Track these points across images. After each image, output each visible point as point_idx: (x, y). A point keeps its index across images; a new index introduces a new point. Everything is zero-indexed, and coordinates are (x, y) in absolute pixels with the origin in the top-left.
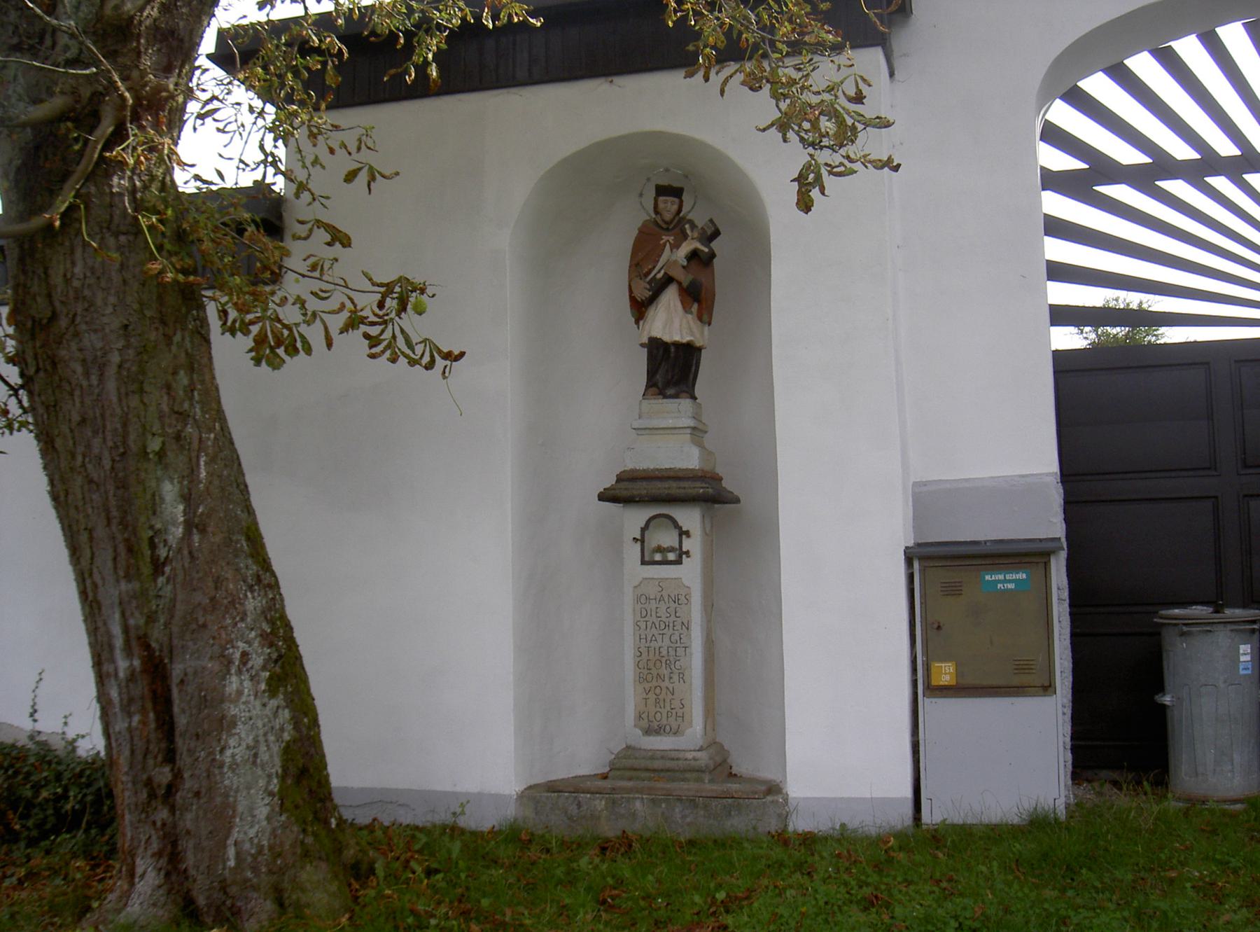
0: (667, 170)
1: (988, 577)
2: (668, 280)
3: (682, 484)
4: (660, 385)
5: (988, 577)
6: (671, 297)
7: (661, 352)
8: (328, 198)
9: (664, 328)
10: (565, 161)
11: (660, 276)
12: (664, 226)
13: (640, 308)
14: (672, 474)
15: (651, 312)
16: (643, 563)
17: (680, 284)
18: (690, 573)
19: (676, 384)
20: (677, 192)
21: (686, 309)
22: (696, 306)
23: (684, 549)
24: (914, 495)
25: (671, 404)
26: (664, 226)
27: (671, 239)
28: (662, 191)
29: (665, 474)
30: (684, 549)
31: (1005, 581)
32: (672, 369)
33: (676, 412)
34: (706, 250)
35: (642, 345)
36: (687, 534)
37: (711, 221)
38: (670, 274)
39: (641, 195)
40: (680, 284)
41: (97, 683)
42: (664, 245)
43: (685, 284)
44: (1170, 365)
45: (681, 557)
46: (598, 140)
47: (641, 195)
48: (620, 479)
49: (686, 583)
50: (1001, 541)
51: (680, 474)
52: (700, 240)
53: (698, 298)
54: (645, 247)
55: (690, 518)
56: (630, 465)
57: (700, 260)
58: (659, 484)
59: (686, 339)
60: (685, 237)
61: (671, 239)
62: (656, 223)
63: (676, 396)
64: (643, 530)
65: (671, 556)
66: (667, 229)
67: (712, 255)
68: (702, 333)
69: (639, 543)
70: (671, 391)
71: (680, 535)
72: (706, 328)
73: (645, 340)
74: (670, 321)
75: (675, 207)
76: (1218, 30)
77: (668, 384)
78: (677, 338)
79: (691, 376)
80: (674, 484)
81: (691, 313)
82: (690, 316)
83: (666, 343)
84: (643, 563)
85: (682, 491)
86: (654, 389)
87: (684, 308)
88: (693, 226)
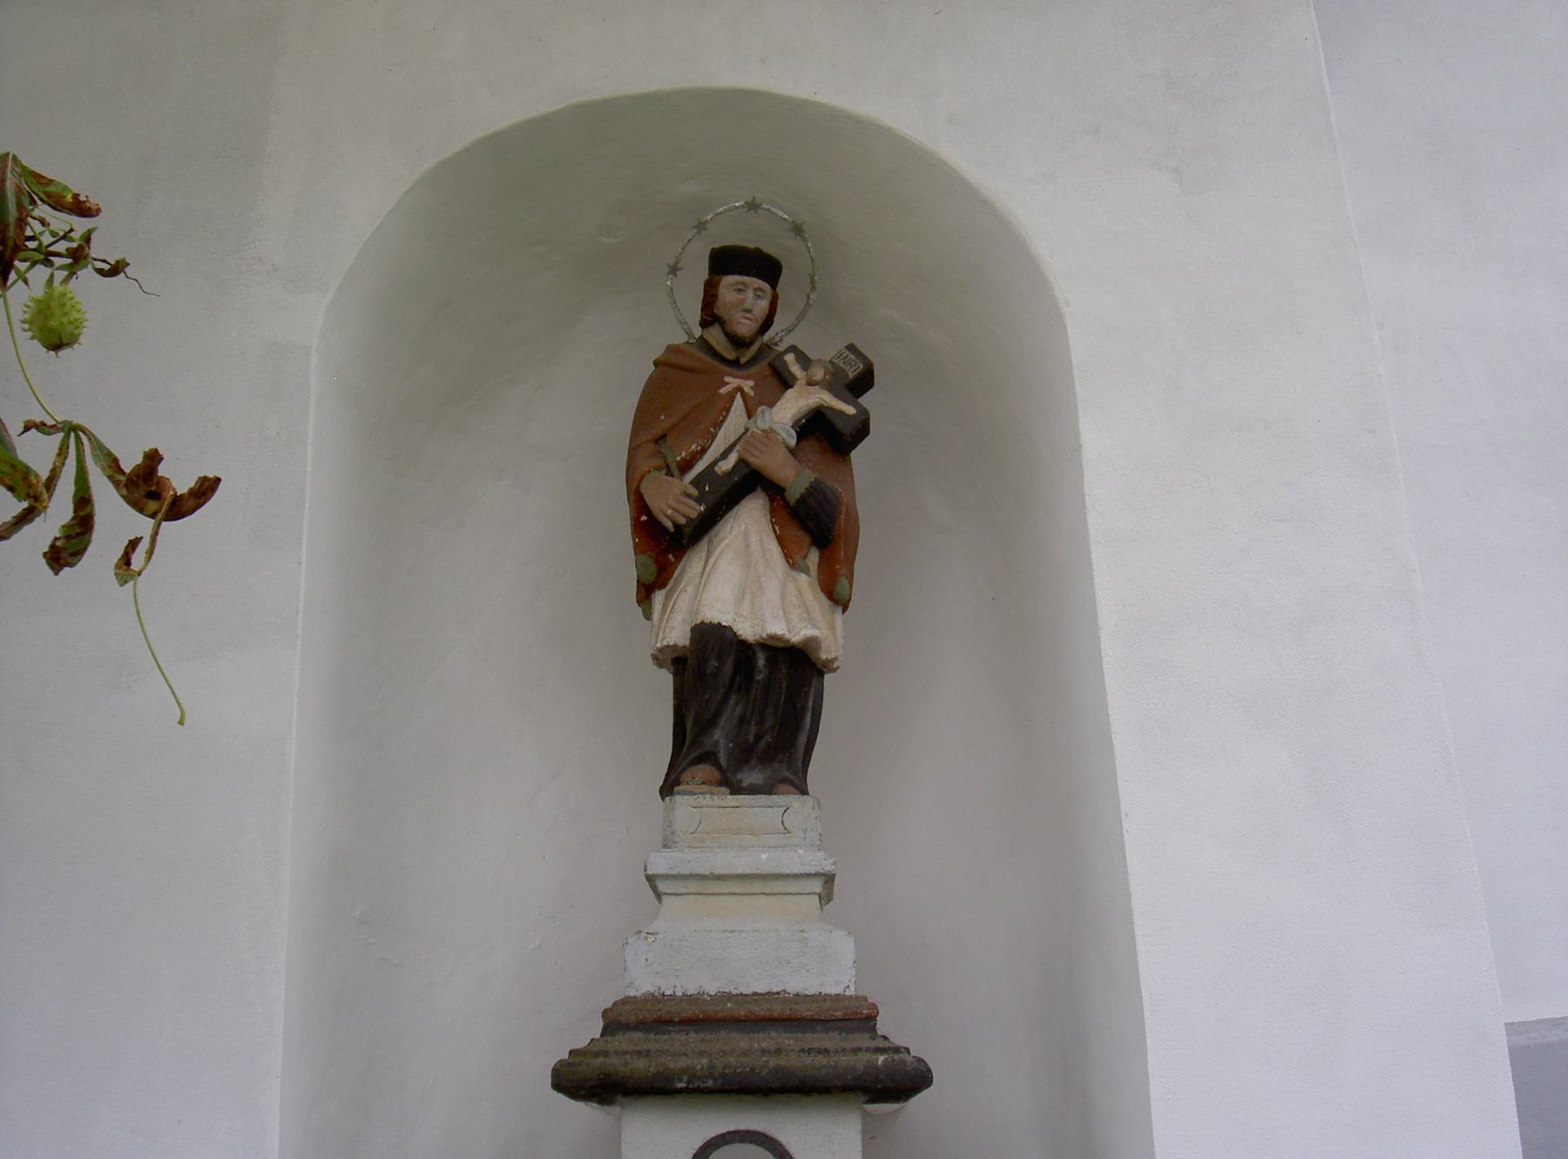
0: (753, 206)
2: (748, 481)
4: (722, 757)
6: (749, 527)
7: (728, 667)
9: (739, 600)
10: (496, 144)
11: (727, 465)
12: (729, 354)
13: (664, 547)
14: (777, 1010)
15: (693, 563)
17: (774, 491)
19: (767, 758)
20: (766, 267)
21: (792, 560)
22: (814, 556)
25: (759, 811)
26: (729, 354)
27: (748, 385)
28: (726, 261)
29: (760, 1010)
32: (744, 715)
33: (748, 831)
35: (660, 657)
37: (851, 348)
39: (674, 270)
41: (675, 734)
42: (731, 398)
43: (795, 492)
44: (670, 1022)
46: (592, 96)
47: (674, 270)
51: (804, 1011)
53: (818, 530)
54: (673, 403)
57: (828, 436)
58: (742, 1040)
59: (798, 633)
60: (785, 382)
61: (748, 385)
62: (704, 344)
63: (768, 789)
66: (735, 364)
67: (862, 429)
68: (832, 626)
70: (752, 777)
72: (839, 618)
73: (677, 634)
74: (745, 584)
75: (763, 305)
77: (745, 755)
78: (776, 627)
79: (802, 740)
80: (788, 1040)
81: (806, 571)
82: (803, 578)
83: (743, 644)
85: (821, 1060)
86: (704, 771)
87: (788, 556)
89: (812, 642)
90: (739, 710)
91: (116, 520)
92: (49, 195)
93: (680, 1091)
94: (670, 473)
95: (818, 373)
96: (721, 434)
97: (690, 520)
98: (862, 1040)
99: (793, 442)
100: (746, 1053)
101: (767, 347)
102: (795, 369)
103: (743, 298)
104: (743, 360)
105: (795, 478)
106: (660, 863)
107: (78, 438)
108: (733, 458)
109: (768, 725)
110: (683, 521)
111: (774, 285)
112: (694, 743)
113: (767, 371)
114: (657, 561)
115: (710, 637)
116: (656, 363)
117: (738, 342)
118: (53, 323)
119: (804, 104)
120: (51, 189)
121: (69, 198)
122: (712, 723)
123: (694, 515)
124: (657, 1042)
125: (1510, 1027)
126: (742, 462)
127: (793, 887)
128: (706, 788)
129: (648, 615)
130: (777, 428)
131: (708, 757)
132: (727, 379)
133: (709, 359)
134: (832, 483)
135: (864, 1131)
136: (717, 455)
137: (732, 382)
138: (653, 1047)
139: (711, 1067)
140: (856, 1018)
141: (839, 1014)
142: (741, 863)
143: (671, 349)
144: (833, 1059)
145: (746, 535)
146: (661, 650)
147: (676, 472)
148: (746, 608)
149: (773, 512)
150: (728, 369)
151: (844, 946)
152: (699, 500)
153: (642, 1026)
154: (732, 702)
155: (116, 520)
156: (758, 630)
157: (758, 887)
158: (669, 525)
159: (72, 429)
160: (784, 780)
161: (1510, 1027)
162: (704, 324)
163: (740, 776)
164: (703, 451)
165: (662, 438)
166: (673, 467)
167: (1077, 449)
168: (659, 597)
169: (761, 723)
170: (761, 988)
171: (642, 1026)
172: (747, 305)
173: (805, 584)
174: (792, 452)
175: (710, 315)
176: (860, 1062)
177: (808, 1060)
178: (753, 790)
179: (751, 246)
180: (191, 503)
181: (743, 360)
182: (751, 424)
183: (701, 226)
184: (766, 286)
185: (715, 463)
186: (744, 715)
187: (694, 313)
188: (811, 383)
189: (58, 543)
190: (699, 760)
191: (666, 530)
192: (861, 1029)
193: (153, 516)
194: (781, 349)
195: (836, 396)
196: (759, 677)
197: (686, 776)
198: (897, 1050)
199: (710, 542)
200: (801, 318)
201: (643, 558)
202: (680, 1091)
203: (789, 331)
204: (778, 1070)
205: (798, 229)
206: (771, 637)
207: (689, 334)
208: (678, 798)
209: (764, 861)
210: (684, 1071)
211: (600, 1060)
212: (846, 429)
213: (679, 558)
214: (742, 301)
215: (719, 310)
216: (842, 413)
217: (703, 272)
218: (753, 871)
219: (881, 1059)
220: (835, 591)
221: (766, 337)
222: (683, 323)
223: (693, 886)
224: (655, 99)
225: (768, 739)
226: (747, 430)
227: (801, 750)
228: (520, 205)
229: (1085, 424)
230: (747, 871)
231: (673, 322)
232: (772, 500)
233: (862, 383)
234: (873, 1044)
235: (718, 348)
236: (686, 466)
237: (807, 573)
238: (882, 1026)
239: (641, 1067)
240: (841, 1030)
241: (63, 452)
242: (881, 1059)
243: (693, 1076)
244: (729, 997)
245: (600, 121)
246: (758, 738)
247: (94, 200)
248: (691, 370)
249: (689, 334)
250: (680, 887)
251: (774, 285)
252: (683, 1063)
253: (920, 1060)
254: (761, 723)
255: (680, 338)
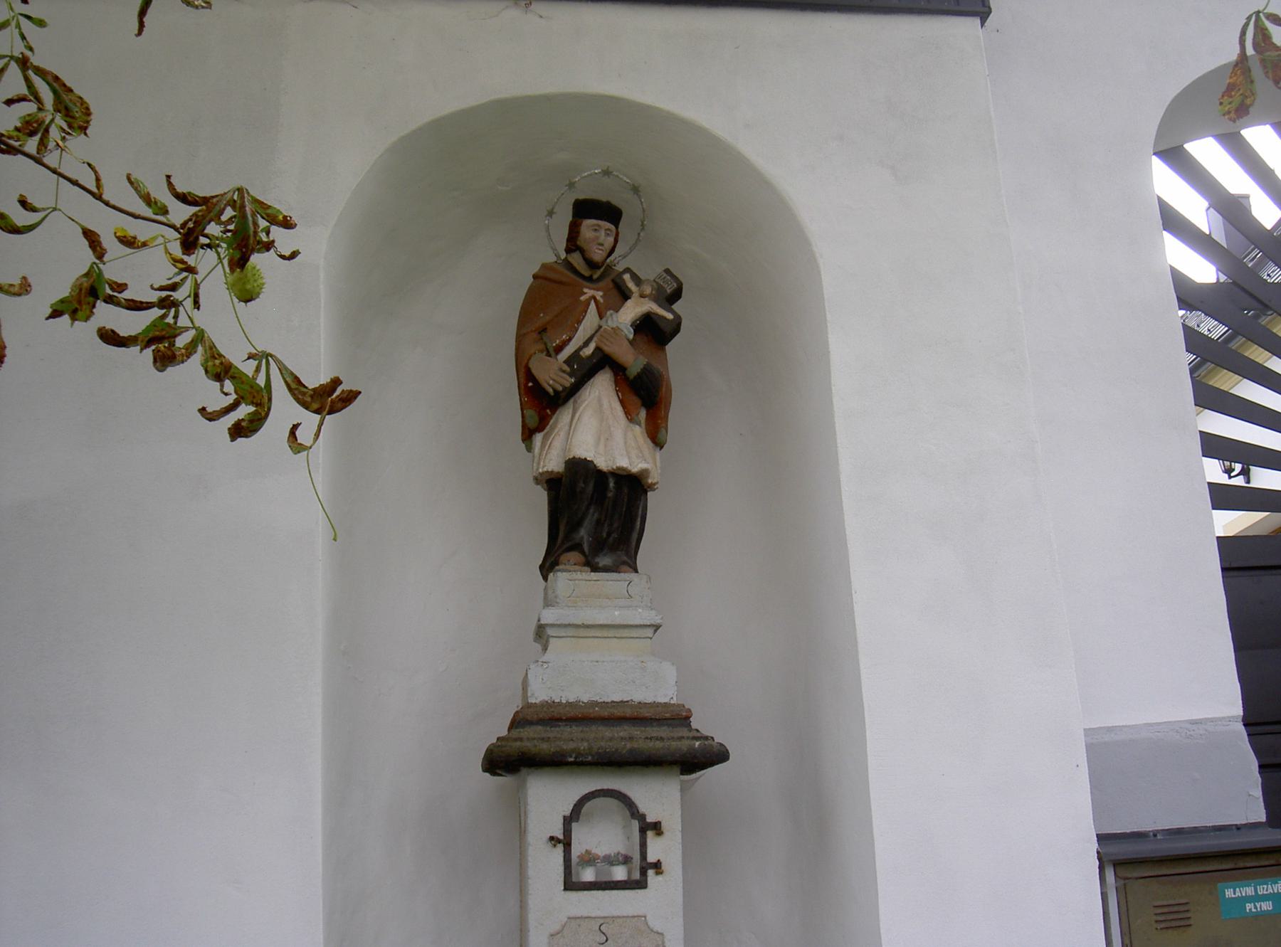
0: (607, 173)
1: (1229, 893)
3: (654, 731)
5: (1229, 893)
6: (601, 393)
8: (41, 23)
10: (437, 126)
11: (588, 351)
12: (586, 273)
13: (542, 405)
14: (628, 712)
15: (563, 417)
16: (571, 885)
17: (618, 370)
18: (660, 903)
19: (614, 548)
20: (611, 214)
22: (643, 414)
23: (651, 858)
24: (1089, 748)
26: (585, 271)
27: (599, 295)
28: (585, 209)
29: (618, 712)
30: (651, 858)
31: (1257, 898)
32: (595, 519)
33: (586, 593)
34: (670, 316)
36: (657, 827)
37: (667, 271)
38: (607, 349)
39: (551, 213)
40: (618, 370)
44: (560, 720)
45: (644, 872)
47: (551, 213)
48: (517, 722)
49: (657, 928)
50: (1179, 832)
51: (646, 713)
52: (656, 299)
53: (646, 396)
54: (547, 305)
55: (658, 796)
56: (539, 694)
57: (654, 332)
58: (607, 732)
60: (625, 295)
62: (569, 265)
64: (568, 821)
65: (620, 873)
66: (589, 279)
67: (676, 327)
69: (560, 847)
70: (604, 561)
71: (644, 829)
72: (658, 454)
73: (554, 463)
74: (597, 431)
76: (1242, 132)
77: (600, 546)
78: (623, 462)
79: (635, 536)
80: (636, 731)
83: (600, 473)
84: (571, 885)
85: (659, 744)
86: (574, 556)
88: (637, 280)
89: (645, 473)
90: (596, 515)
91: (285, 410)
92: (268, 215)
93: (571, 764)
94: (549, 355)
95: (648, 290)
96: (581, 328)
97: (565, 388)
98: (683, 732)
99: (631, 336)
100: (611, 739)
101: (609, 267)
102: (631, 285)
103: (595, 233)
104: (595, 277)
105: (634, 361)
106: (549, 616)
107: (268, 363)
108: (592, 346)
109: (615, 525)
110: (560, 389)
111: (617, 228)
112: (567, 537)
113: (611, 285)
114: (539, 413)
115: (579, 468)
116: (535, 277)
117: (592, 265)
118: (249, 287)
119: (649, 107)
120: (269, 211)
121: (281, 217)
122: (579, 524)
123: (568, 385)
124: (552, 732)
125: (1088, 732)
126: (598, 349)
127: (635, 633)
128: (577, 567)
129: (529, 449)
130: (621, 326)
131: (577, 547)
132: (585, 290)
133: (569, 274)
134: (656, 365)
135: (682, 790)
136: (581, 343)
137: (589, 292)
138: (551, 735)
139: (590, 748)
140: (679, 718)
141: (668, 715)
142: (602, 619)
143: (544, 266)
144: (667, 744)
145: (599, 400)
146: (541, 474)
147: (552, 353)
148: (601, 447)
149: (617, 383)
150: (585, 283)
151: (669, 672)
152: (571, 375)
153: (541, 722)
154: (591, 511)
155: (285, 410)
156: (610, 464)
157: (611, 633)
158: (551, 391)
159: (267, 356)
160: (624, 563)
161: (1088, 732)
162: (568, 251)
163: (597, 560)
164: (570, 339)
165: (543, 330)
166: (551, 351)
167: (826, 354)
168: (538, 438)
169: (611, 525)
170: (617, 698)
171: (541, 722)
172: (601, 241)
173: (638, 433)
174: (631, 343)
175: (573, 244)
176: (684, 745)
177: (651, 744)
178: (606, 569)
179: (604, 199)
180: (340, 405)
181: (595, 277)
182: (603, 323)
183: (571, 185)
184: (613, 227)
185: (581, 348)
186: (595, 519)
187: (561, 246)
188: (642, 296)
189: (244, 424)
190: (569, 549)
191: (547, 393)
192: (682, 725)
193: (317, 412)
194: (620, 268)
195: (660, 306)
196: (610, 494)
197: (563, 558)
198: (706, 738)
199: (575, 402)
200: (631, 250)
201: (529, 412)
202: (571, 764)
203: (625, 257)
204: (631, 751)
205: (636, 190)
206: (619, 468)
207: (557, 256)
208: (559, 574)
209: (617, 616)
210: (573, 751)
211: (518, 743)
212: (668, 329)
213: (554, 412)
214: (597, 238)
215: (580, 242)
216: (665, 318)
217: (565, 216)
218: (609, 622)
219: (697, 744)
220: (656, 436)
221: (612, 258)
222: (554, 250)
223: (571, 632)
224: (548, 99)
225: (615, 535)
226: (600, 327)
227: (634, 544)
228: (451, 167)
229: (832, 339)
230: (605, 622)
231: (546, 248)
232: (616, 375)
233: (676, 295)
234: (691, 735)
235: (576, 265)
236: (559, 349)
237: (639, 425)
238: (695, 723)
239: (545, 748)
240: (669, 725)
241: (258, 370)
242: (697, 744)
243: (579, 754)
244: (596, 704)
245: (509, 113)
246: (609, 535)
247: (295, 219)
248: (561, 283)
249: (557, 256)
250: (562, 632)
251: (617, 228)
252: (572, 745)
253: (721, 745)
254: (611, 525)
255: (551, 259)
